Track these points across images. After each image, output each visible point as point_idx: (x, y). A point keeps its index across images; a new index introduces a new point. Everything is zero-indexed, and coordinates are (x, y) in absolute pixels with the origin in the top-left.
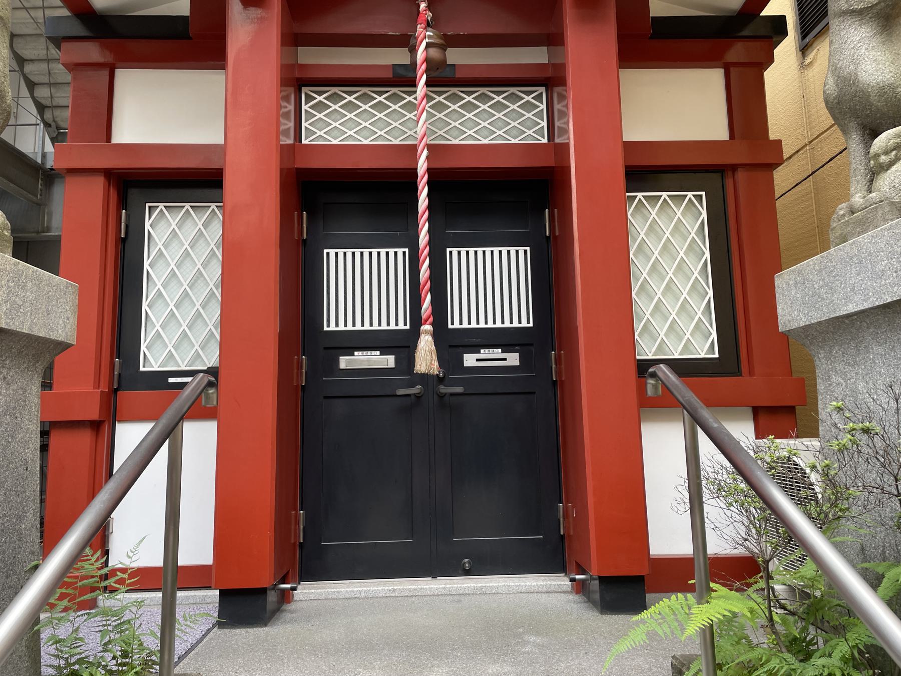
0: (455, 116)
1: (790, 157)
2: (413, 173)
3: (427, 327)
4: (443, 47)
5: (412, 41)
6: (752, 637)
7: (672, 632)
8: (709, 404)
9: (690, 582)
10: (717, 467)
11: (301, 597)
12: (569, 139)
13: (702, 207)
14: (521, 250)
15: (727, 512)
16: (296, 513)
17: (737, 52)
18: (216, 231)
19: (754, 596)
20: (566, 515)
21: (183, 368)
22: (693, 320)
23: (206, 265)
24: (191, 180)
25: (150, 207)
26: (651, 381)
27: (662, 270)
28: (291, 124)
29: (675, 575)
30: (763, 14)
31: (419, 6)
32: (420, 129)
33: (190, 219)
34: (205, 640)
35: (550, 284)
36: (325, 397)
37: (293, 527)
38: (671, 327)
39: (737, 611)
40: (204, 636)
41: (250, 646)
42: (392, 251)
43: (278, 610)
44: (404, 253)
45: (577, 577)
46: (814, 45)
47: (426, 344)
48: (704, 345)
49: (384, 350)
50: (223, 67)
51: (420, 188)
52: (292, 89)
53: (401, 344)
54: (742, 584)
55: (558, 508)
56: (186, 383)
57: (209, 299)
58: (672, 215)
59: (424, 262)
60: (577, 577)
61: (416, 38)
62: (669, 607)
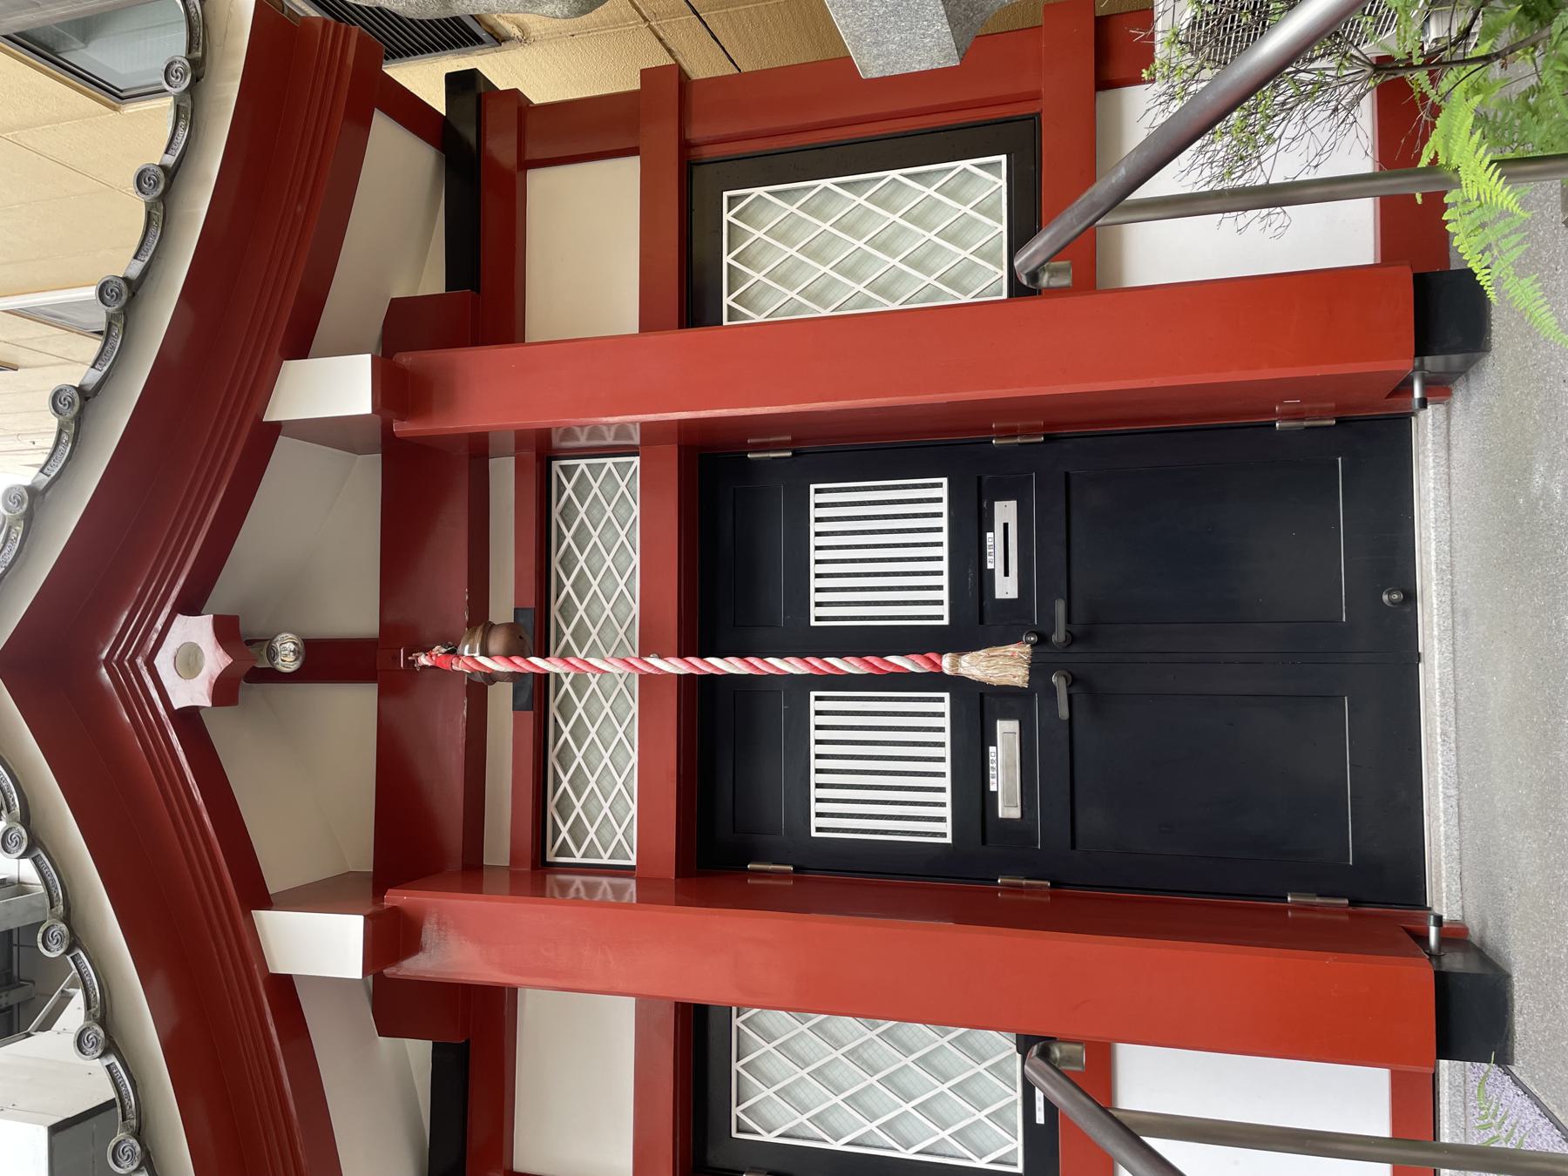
0: (596, 609)
1: (669, 51)
2: (685, 681)
3: (946, 663)
4: (489, 628)
5: (479, 679)
6: (1524, 86)
7: (1516, 231)
8: (1091, 179)
9: (1419, 201)
10: (1201, 160)
11: (1456, 907)
12: (634, 423)
13: (748, 196)
14: (814, 498)
15: (1284, 142)
16: (1292, 909)
17: (501, 148)
18: (781, 1021)
19: (1444, 86)
20: (1297, 415)
21: (1018, 1095)
22: (939, 201)
23: (837, 1041)
24: (694, 1055)
25: (739, 1131)
26: (1045, 280)
27: (854, 259)
28: (605, 881)
29: (1413, 225)
30: (441, 108)
31: (424, 667)
32: (615, 668)
33: (759, 1063)
34: (1535, 1090)
35: (875, 450)
36: (1073, 847)
37: (1319, 916)
38: (952, 239)
39: (1471, 119)
40: (1526, 1091)
41: (1547, 1008)
42: (815, 720)
43: (1480, 953)
44: (817, 698)
45: (1417, 394)
46: (491, 22)
47: (977, 666)
48: (986, 181)
49: (987, 738)
50: (514, 991)
51: (709, 670)
52: (550, 878)
53: (977, 709)
54: (1423, 107)
55: (1284, 431)
56: (1047, 1102)
57: (896, 1041)
58: (760, 245)
59: (833, 667)
60: (1417, 394)
61: (474, 672)
62: (1468, 236)
